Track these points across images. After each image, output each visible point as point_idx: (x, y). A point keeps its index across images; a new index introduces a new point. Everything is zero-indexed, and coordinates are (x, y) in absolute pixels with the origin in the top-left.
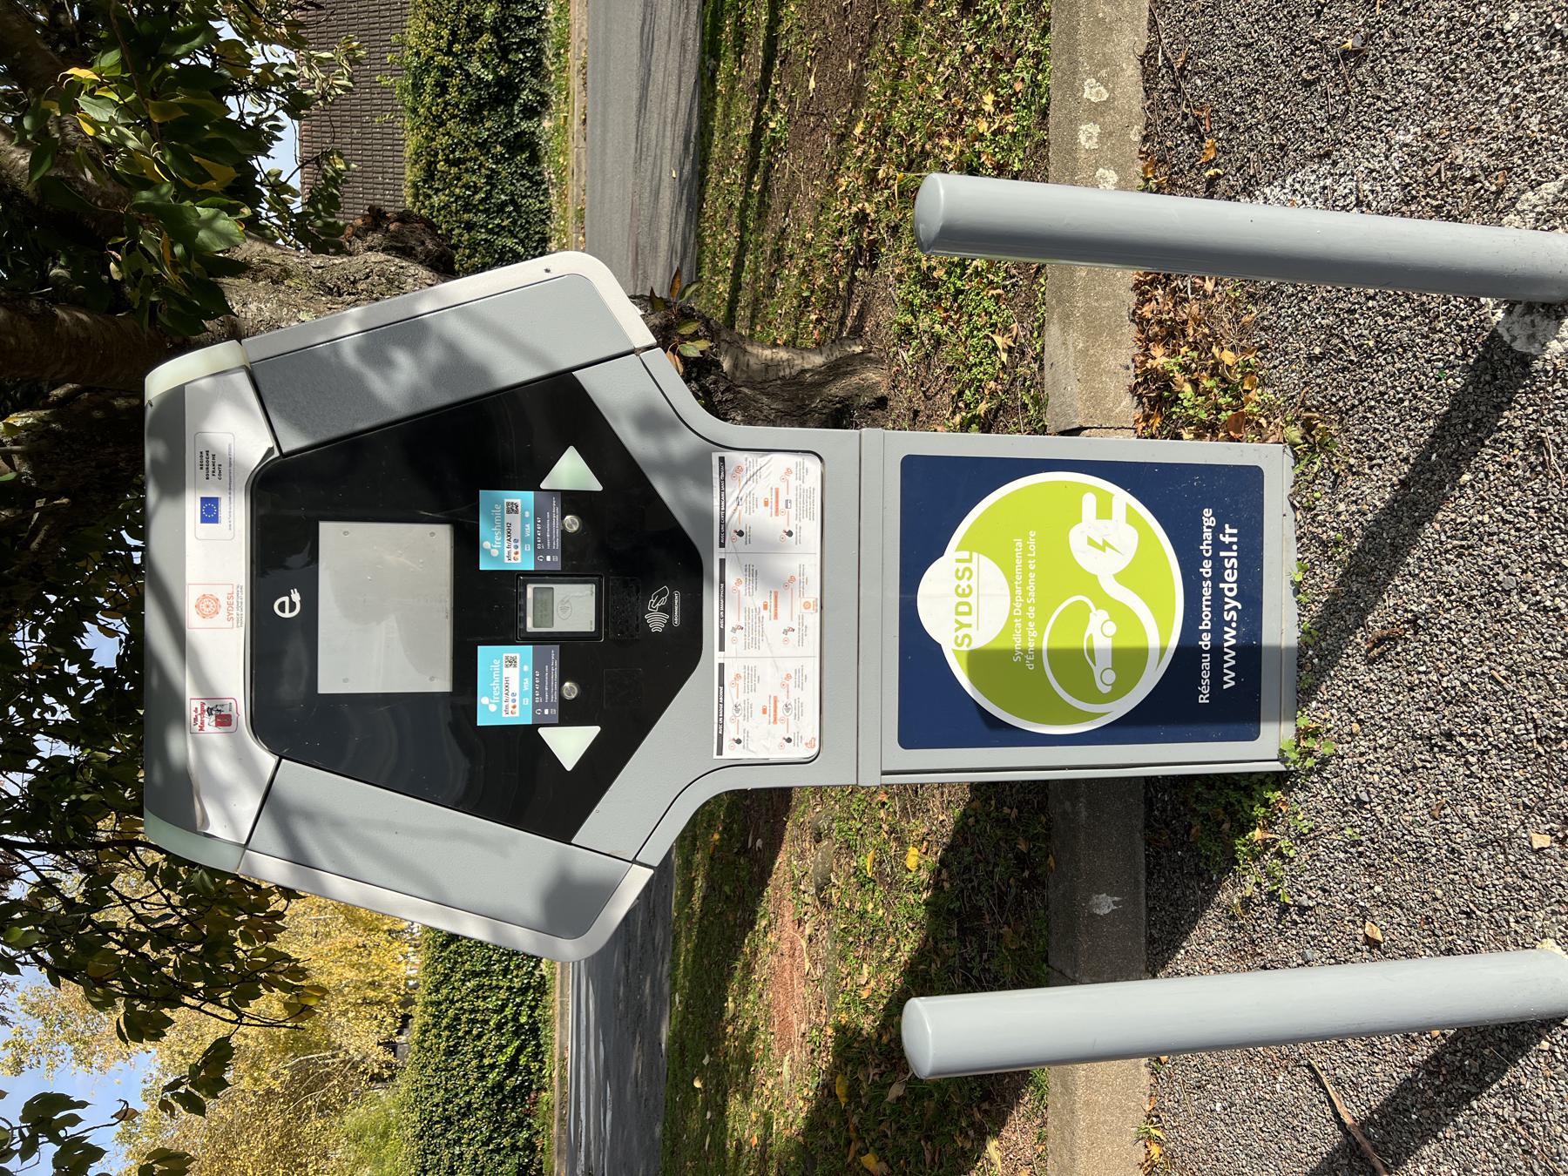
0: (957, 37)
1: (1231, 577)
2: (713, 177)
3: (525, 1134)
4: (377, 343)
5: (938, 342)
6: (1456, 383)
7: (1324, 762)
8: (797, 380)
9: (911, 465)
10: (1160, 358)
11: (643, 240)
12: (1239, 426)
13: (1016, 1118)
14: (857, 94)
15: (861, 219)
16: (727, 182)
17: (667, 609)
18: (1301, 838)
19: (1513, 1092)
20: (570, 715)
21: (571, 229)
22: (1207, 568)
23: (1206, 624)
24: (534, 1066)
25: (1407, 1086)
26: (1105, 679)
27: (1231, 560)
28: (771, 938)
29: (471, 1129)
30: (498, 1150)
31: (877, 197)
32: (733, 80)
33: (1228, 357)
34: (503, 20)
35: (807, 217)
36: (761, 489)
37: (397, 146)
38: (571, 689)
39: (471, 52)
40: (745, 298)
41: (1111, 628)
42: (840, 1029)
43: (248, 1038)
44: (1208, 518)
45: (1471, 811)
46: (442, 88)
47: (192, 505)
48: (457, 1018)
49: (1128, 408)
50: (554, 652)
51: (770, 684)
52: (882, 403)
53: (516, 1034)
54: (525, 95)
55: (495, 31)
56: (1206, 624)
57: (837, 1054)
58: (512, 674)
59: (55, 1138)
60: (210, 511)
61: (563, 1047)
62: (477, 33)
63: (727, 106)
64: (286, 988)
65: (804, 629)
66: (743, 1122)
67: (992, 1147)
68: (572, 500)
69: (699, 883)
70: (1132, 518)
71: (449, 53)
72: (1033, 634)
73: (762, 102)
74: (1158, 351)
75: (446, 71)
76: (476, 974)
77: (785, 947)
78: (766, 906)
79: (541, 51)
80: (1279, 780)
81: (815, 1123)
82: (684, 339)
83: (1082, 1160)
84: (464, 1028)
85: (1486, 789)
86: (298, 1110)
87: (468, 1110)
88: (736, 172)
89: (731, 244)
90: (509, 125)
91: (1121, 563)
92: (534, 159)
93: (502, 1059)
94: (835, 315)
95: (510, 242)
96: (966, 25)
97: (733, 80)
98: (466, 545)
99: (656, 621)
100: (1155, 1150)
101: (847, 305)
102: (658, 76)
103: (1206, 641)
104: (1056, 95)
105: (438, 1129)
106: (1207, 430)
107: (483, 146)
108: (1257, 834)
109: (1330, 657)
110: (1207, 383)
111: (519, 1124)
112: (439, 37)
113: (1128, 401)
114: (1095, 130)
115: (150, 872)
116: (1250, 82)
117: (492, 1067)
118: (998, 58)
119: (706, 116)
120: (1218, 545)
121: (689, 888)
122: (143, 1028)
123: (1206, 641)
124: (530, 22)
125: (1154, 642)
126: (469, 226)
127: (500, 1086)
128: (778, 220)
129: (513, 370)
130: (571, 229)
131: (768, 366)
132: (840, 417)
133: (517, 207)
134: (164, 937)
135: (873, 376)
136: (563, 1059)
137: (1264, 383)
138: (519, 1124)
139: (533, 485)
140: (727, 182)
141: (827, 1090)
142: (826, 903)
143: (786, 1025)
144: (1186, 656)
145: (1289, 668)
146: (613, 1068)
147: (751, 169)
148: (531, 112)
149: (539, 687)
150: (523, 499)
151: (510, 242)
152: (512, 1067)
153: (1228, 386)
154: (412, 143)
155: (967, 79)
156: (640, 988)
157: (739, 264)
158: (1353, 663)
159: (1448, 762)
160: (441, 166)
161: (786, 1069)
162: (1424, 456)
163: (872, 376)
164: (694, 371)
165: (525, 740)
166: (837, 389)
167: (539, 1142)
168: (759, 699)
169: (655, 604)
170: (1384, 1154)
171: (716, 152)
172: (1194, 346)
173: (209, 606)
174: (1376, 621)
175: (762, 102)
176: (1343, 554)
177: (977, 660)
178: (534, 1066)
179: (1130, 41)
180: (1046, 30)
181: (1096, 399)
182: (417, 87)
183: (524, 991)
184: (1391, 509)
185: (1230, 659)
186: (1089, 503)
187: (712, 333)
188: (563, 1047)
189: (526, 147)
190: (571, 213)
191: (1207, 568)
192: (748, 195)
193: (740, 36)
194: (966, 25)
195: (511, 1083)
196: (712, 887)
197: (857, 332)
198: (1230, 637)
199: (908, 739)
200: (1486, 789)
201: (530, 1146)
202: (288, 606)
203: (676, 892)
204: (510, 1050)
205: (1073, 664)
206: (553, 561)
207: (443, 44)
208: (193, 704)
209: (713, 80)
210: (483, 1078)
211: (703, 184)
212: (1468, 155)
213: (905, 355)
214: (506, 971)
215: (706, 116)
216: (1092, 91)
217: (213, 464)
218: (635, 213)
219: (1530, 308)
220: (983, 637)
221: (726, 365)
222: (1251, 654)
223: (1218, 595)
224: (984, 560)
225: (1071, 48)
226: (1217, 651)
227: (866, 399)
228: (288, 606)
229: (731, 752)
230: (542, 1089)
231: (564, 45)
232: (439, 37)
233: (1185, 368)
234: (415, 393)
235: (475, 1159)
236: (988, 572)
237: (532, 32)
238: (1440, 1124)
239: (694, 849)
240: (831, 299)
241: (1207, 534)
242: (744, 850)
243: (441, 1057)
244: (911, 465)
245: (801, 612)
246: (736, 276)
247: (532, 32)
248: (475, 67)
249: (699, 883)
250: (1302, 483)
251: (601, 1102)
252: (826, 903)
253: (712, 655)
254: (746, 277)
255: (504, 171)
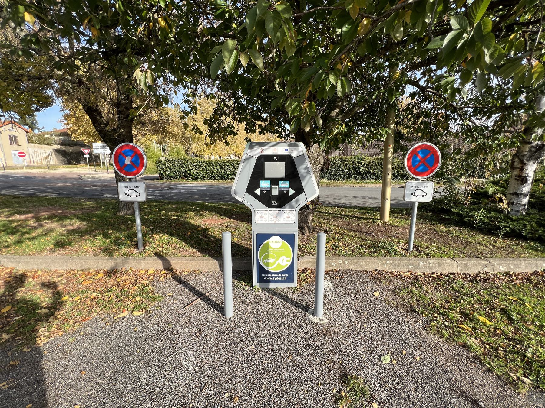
0: (357, 244)
1: (279, 279)
2: (341, 209)
3: (178, 177)
4: (307, 168)
5: (312, 242)
6: (305, 305)
7: (254, 291)
8: (307, 222)
9: (294, 235)
10: (309, 272)
11: (332, 197)
12: (299, 281)
13: (200, 253)
14: (352, 230)
15: (331, 231)
16: (340, 211)
17: (275, 203)
18: (244, 289)
19: (214, 311)
20: (262, 192)
21: (335, 184)
22: (280, 275)
23: (273, 275)
24: (190, 179)
25: (212, 301)
26: (265, 261)
27: (281, 279)
28: (220, 219)
29: (180, 168)
30: (176, 172)
31: (334, 234)
32: (356, 212)
33: (309, 280)
34: (371, 173)
35: (333, 224)
36: (290, 215)
37: (349, 155)
38: (265, 192)
39: (365, 167)
40: (321, 214)
41: (272, 262)
42: (208, 229)
43: (203, 136)
44: (287, 275)
45: (249, 307)
46: (359, 163)
47: (288, 148)
48: (199, 165)
49: (302, 268)
50: (270, 190)
51: (265, 217)
52: (304, 234)
53: (196, 175)
54: (358, 176)
55: (368, 172)
56: (273, 275)
57: (204, 228)
58: (267, 185)
59: (191, 111)
60: (286, 150)
61: (193, 183)
62: (368, 168)
63: (352, 211)
64: (210, 142)
65: (272, 221)
66: (191, 214)
67: (195, 250)
68: (288, 192)
69: (226, 207)
70: (287, 265)
71: (365, 164)
72: (272, 251)
73: (351, 217)
74: (310, 271)
75: (361, 163)
76: (206, 169)
77: (219, 221)
78: (224, 218)
79: (366, 179)
80: (251, 286)
81: (193, 225)
82: (312, 205)
83: (196, 262)
84: (197, 167)
85: (252, 308)
86: (181, 137)
87: (183, 167)
88: (341, 213)
89: (330, 212)
90: (353, 174)
91: (281, 263)
92: (347, 178)
93: (192, 173)
94: (318, 228)
95: (333, 174)
96: (358, 246)
97: (356, 212)
98: (282, 179)
99: (273, 202)
100: (198, 272)
101: (319, 229)
102: (359, 200)
103: (270, 275)
104: (346, 257)
105: (180, 162)
106: (299, 277)
107: (349, 169)
108: (244, 283)
109: (268, 292)
110: (305, 277)
111: (180, 176)
112: (367, 162)
113: (303, 268)
114: (341, 262)
115: (230, 122)
116: (346, 282)
117: (190, 171)
118: (353, 250)
119: (351, 208)
120: (283, 277)
121: (225, 205)
122: (206, 122)
123: (270, 275)
124: (370, 177)
125: (270, 268)
126: (335, 167)
127: (187, 173)
128: (333, 219)
129: (303, 184)
130: (335, 184)
131: (309, 217)
132: (301, 227)
133: (339, 175)
134: (219, 125)
135: (307, 233)
136: (191, 183)
137: (305, 284)
138: (180, 176)
139: (290, 187)
140: (340, 211)
141: (199, 227)
142: (227, 227)
143: (207, 221)
144: (268, 272)
145: (267, 287)
146: (192, 193)
147: (341, 215)
148: (355, 177)
149: (265, 188)
150: (288, 186)
151: (333, 174)
152: (190, 175)
153: (304, 280)
154: (349, 157)
155: (350, 246)
156: (207, 197)
157: (327, 213)
158: (268, 294)
159: (255, 304)
160: (345, 162)
161: (200, 221)
162: (295, 302)
163: (308, 233)
164: (307, 206)
165: (259, 186)
166: (306, 227)
167: (177, 179)
168: (263, 215)
169: (275, 202)
170: (203, 298)
171: (345, 209)
172: (311, 276)
173: (275, 150)
174: (273, 297)
175: (351, 217)
176: (282, 293)
177: (268, 244)
178: (190, 179)
179: (354, 267)
180: (356, 256)
181: (303, 263)
182: (358, 159)
183: (203, 177)
184: (288, 298)
185: (268, 278)
186: (289, 259)
187: (313, 209)
188: (193, 183)
189: (349, 177)
190: (338, 184)
191: (280, 275)
192: (337, 214)
193: (362, 213)
194: (358, 246)
195: (188, 175)
196: (226, 209)
197: (314, 231)
198: (271, 278)
199: (258, 235)
200: (252, 308)
201: (176, 178)
202: (275, 159)
203: (224, 203)
204: (193, 174)
205: (267, 257)
206: (281, 190)
207: (366, 163)
208: (263, 148)
209: (356, 209)
210: (188, 170)
211: (340, 207)
212: (334, 306)
213: (311, 238)
214: (207, 174)
215: (351, 208)
216: (346, 262)
217: (292, 150)
218: (337, 196)
219: (314, 312)
220: (271, 245)
221: (309, 211)
222: (268, 281)
223: (276, 277)
224: (281, 245)
225: (353, 259)
226: (269, 277)
227: (304, 232)
228: (275, 159)
229: (256, 212)
230: (186, 180)
231: (367, 183)
232: (367, 162)
233: (307, 274)
234: (300, 172)
235: (175, 169)
236: (279, 245)
237: (369, 178)
238: (208, 304)
239: (232, 206)
240: (320, 227)
241: (284, 275)
242: (233, 214)
243: (192, 163)
244: (294, 235)
245: (275, 220)
246: (325, 213)
247: (369, 178)
248: (362, 168)
249: (226, 207)
250: (292, 289)
251: (185, 190)
252: (227, 227)
253: (269, 209)
254: (324, 214)
255: (345, 173)
